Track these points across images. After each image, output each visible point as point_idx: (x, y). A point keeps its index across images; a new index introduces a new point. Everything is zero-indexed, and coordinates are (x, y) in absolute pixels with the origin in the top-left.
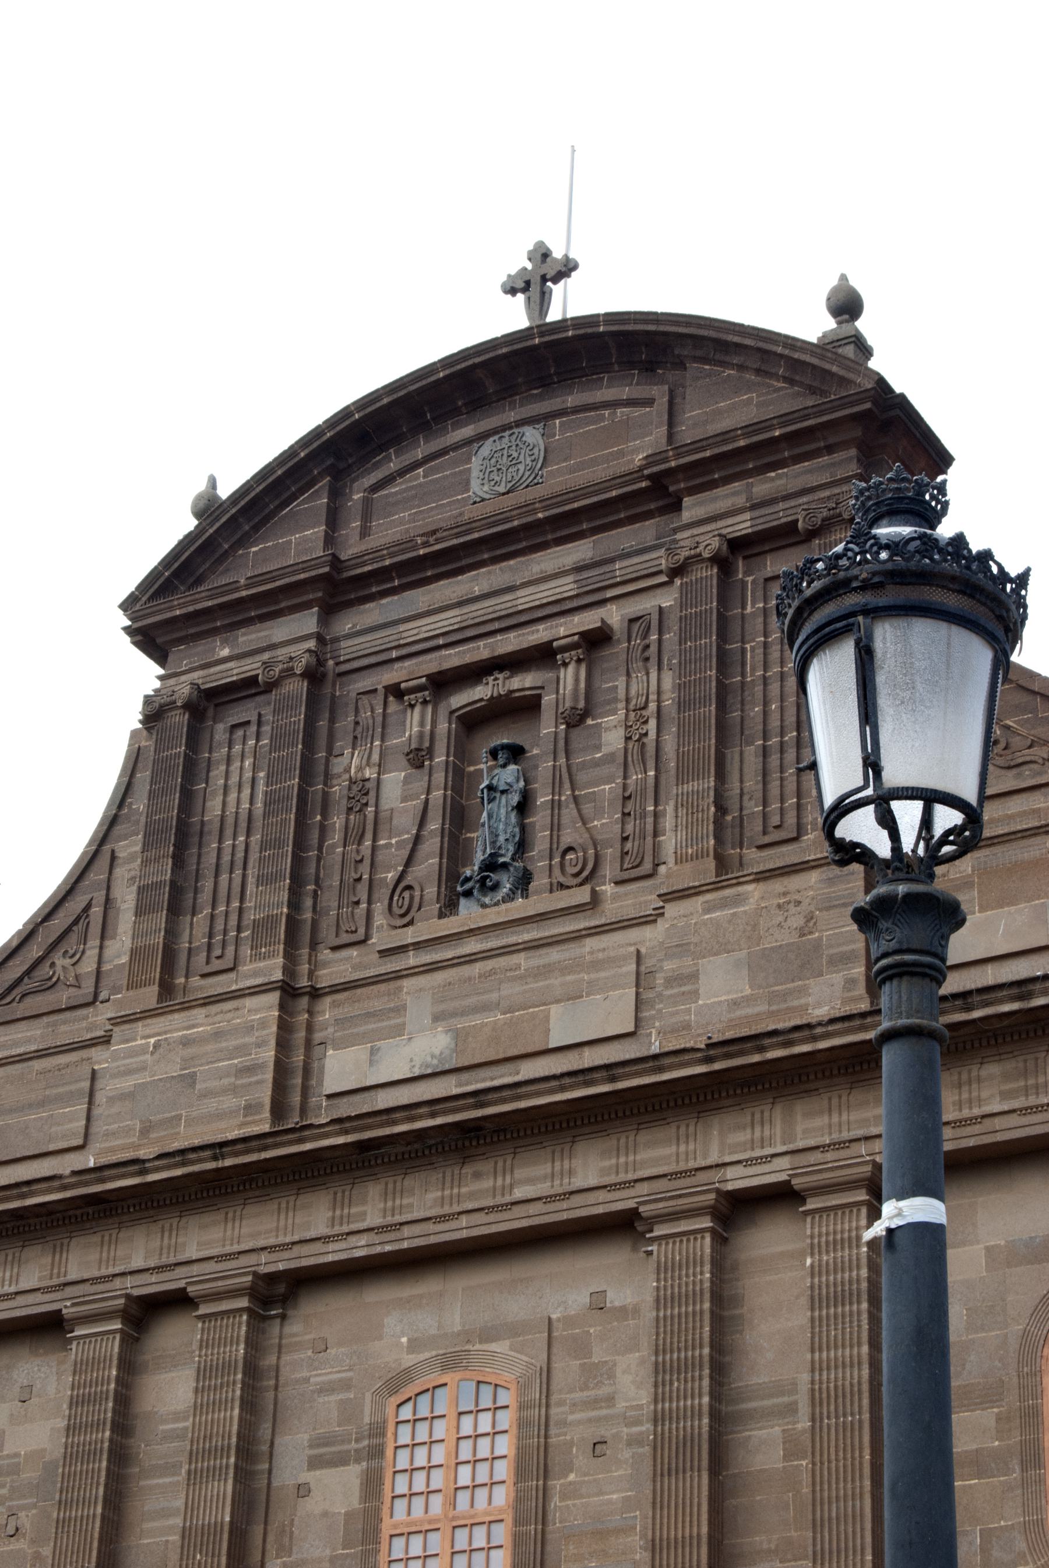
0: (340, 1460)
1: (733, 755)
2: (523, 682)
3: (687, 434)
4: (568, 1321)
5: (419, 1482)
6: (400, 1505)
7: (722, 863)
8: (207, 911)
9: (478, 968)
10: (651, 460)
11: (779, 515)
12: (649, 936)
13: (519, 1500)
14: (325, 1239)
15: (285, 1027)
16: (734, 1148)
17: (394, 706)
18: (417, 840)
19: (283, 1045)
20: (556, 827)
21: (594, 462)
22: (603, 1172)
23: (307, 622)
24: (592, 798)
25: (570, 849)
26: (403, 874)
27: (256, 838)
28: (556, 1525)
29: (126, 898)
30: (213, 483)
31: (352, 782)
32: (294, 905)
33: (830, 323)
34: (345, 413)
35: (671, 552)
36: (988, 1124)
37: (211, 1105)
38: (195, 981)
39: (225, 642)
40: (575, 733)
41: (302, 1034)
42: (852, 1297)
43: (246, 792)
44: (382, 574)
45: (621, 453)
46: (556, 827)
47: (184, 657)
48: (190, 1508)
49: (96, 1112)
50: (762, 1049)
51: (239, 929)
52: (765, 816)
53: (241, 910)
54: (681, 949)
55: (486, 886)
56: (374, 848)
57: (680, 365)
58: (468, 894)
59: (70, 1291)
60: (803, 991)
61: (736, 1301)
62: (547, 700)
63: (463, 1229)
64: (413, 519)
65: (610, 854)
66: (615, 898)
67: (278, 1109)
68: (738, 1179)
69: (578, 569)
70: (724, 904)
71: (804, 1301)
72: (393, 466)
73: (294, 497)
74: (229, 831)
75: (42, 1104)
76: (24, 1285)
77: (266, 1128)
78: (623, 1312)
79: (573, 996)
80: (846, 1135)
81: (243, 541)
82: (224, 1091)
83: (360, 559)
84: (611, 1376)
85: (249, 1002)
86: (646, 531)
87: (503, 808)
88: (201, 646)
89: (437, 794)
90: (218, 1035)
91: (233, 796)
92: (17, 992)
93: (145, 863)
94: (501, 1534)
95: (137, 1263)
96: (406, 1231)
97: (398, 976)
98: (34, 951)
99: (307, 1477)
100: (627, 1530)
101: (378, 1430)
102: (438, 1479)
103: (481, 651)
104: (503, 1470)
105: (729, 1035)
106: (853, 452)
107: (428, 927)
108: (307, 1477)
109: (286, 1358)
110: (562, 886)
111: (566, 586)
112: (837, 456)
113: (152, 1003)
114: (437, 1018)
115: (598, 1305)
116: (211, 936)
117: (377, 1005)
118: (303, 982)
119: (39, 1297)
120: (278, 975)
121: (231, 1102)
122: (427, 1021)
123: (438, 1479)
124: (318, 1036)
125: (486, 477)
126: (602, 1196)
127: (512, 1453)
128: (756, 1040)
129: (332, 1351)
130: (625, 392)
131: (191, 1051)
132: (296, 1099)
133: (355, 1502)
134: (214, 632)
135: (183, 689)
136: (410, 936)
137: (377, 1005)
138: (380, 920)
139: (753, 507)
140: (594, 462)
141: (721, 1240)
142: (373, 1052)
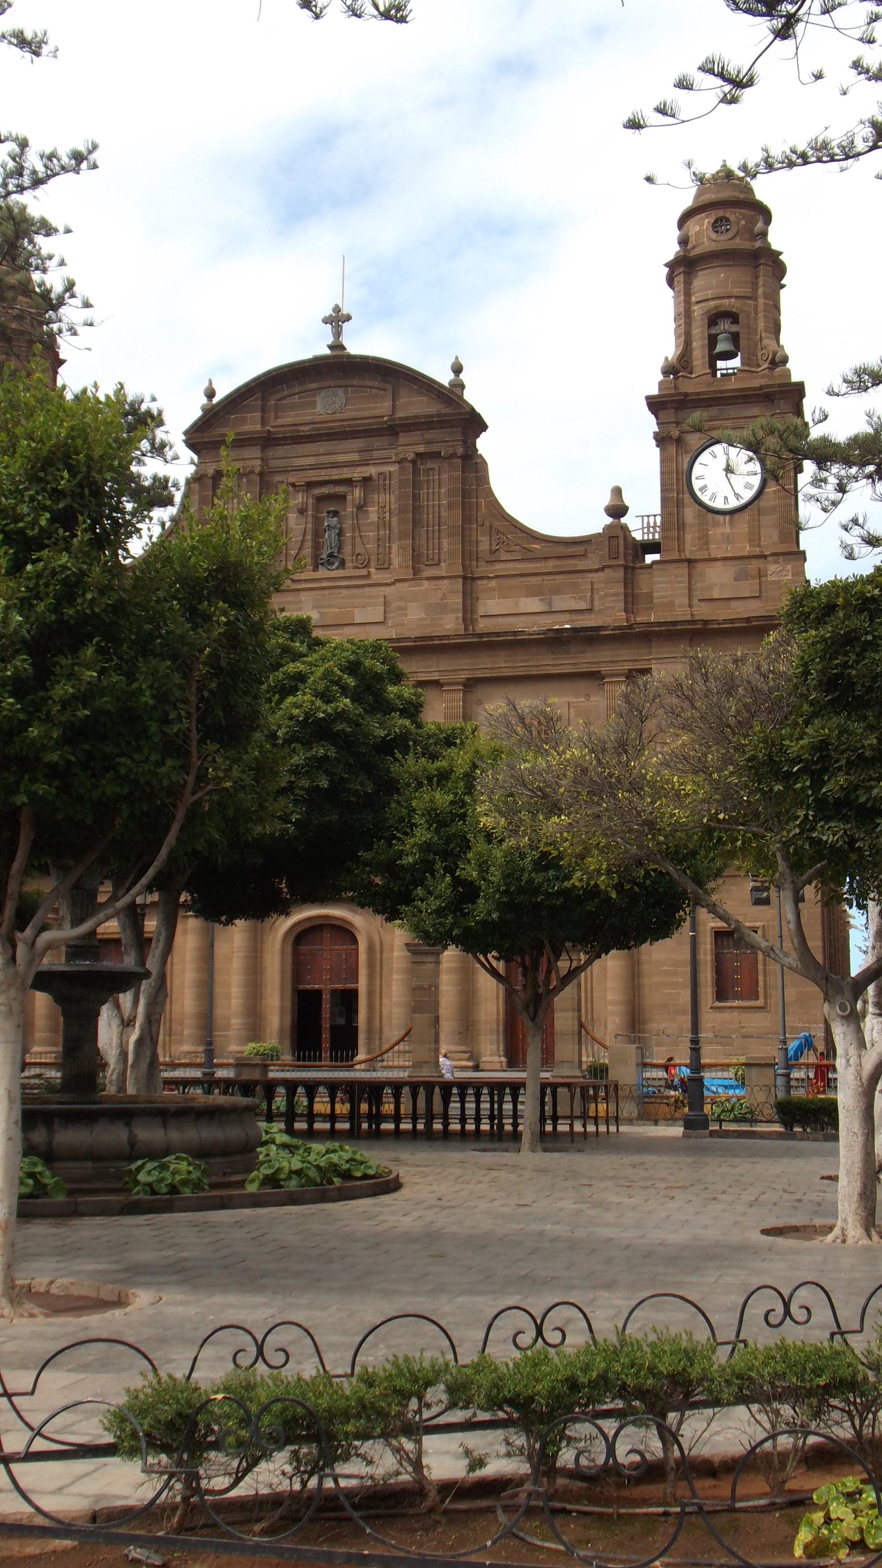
11: (435, 448)
18: (303, 541)
20: (354, 545)
46: (354, 545)
58: (322, 564)
62: (349, 498)
81: (229, 413)
89: (310, 526)
110: (357, 567)
111: (355, 457)
128: (431, 638)
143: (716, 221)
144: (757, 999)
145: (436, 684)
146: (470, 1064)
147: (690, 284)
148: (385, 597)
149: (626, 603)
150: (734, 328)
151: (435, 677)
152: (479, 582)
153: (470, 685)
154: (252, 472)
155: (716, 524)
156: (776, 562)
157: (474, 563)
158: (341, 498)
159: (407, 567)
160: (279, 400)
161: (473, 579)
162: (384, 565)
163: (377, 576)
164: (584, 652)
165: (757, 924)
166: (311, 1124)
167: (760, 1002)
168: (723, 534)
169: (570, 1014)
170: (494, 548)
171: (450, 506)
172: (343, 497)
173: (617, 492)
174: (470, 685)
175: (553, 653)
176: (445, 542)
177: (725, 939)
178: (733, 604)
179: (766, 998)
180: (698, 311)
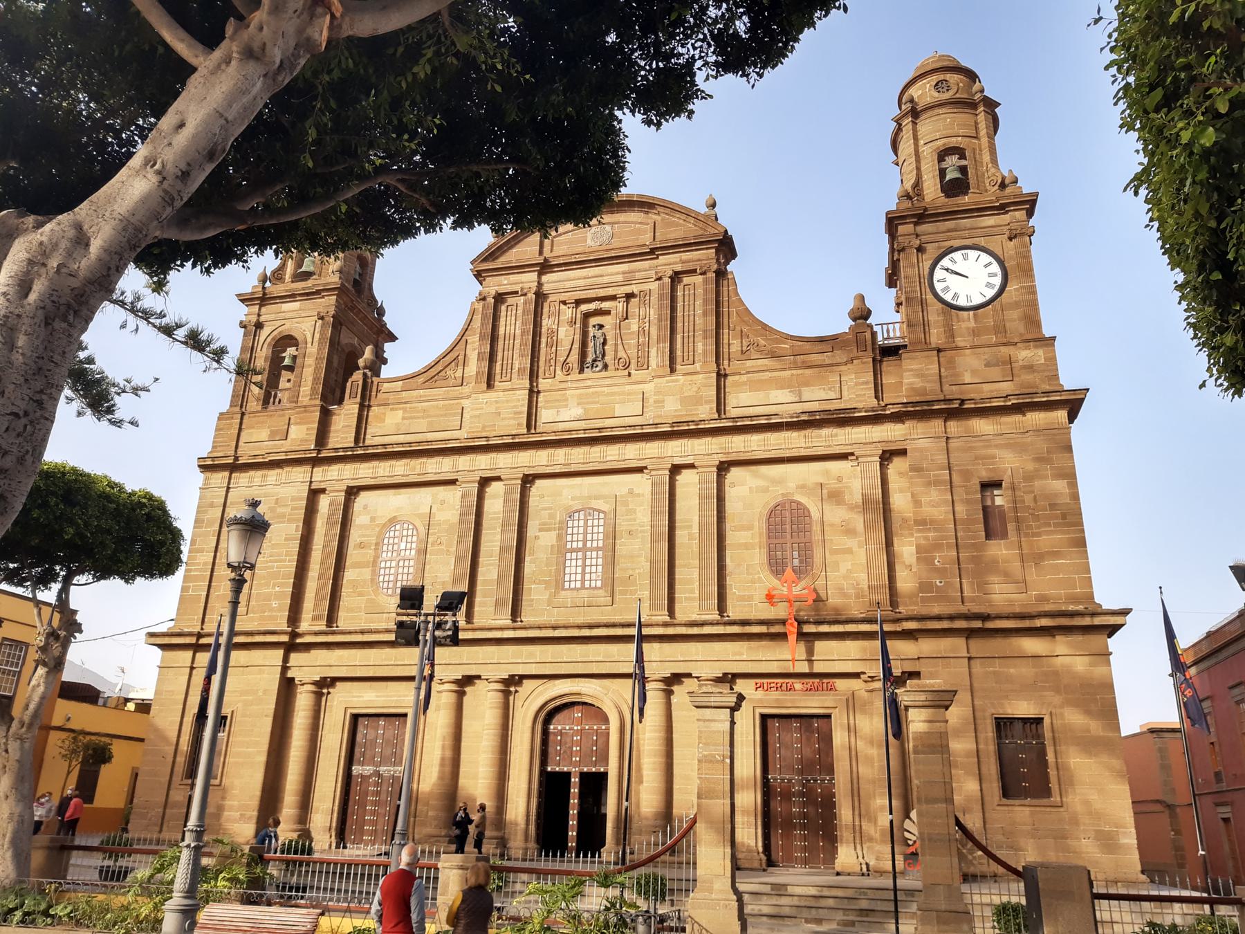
0: (549, 530)
2: (605, 305)
4: (622, 496)
20: (616, 351)
24: (628, 344)
29: (473, 356)
37: (506, 422)
46: (616, 351)
65: (633, 362)
69: (624, 273)
70: (673, 381)
75: (445, 415)
78: (638, 495)
82: (510, 418)
84: (635, 512)
98: (439, 367)
99: (537, 534)
111: (620, 278)
121: (512, 422)
125: (593, 239)
138: (558, 371)
156: (1026, 348)
168: (968, 328)
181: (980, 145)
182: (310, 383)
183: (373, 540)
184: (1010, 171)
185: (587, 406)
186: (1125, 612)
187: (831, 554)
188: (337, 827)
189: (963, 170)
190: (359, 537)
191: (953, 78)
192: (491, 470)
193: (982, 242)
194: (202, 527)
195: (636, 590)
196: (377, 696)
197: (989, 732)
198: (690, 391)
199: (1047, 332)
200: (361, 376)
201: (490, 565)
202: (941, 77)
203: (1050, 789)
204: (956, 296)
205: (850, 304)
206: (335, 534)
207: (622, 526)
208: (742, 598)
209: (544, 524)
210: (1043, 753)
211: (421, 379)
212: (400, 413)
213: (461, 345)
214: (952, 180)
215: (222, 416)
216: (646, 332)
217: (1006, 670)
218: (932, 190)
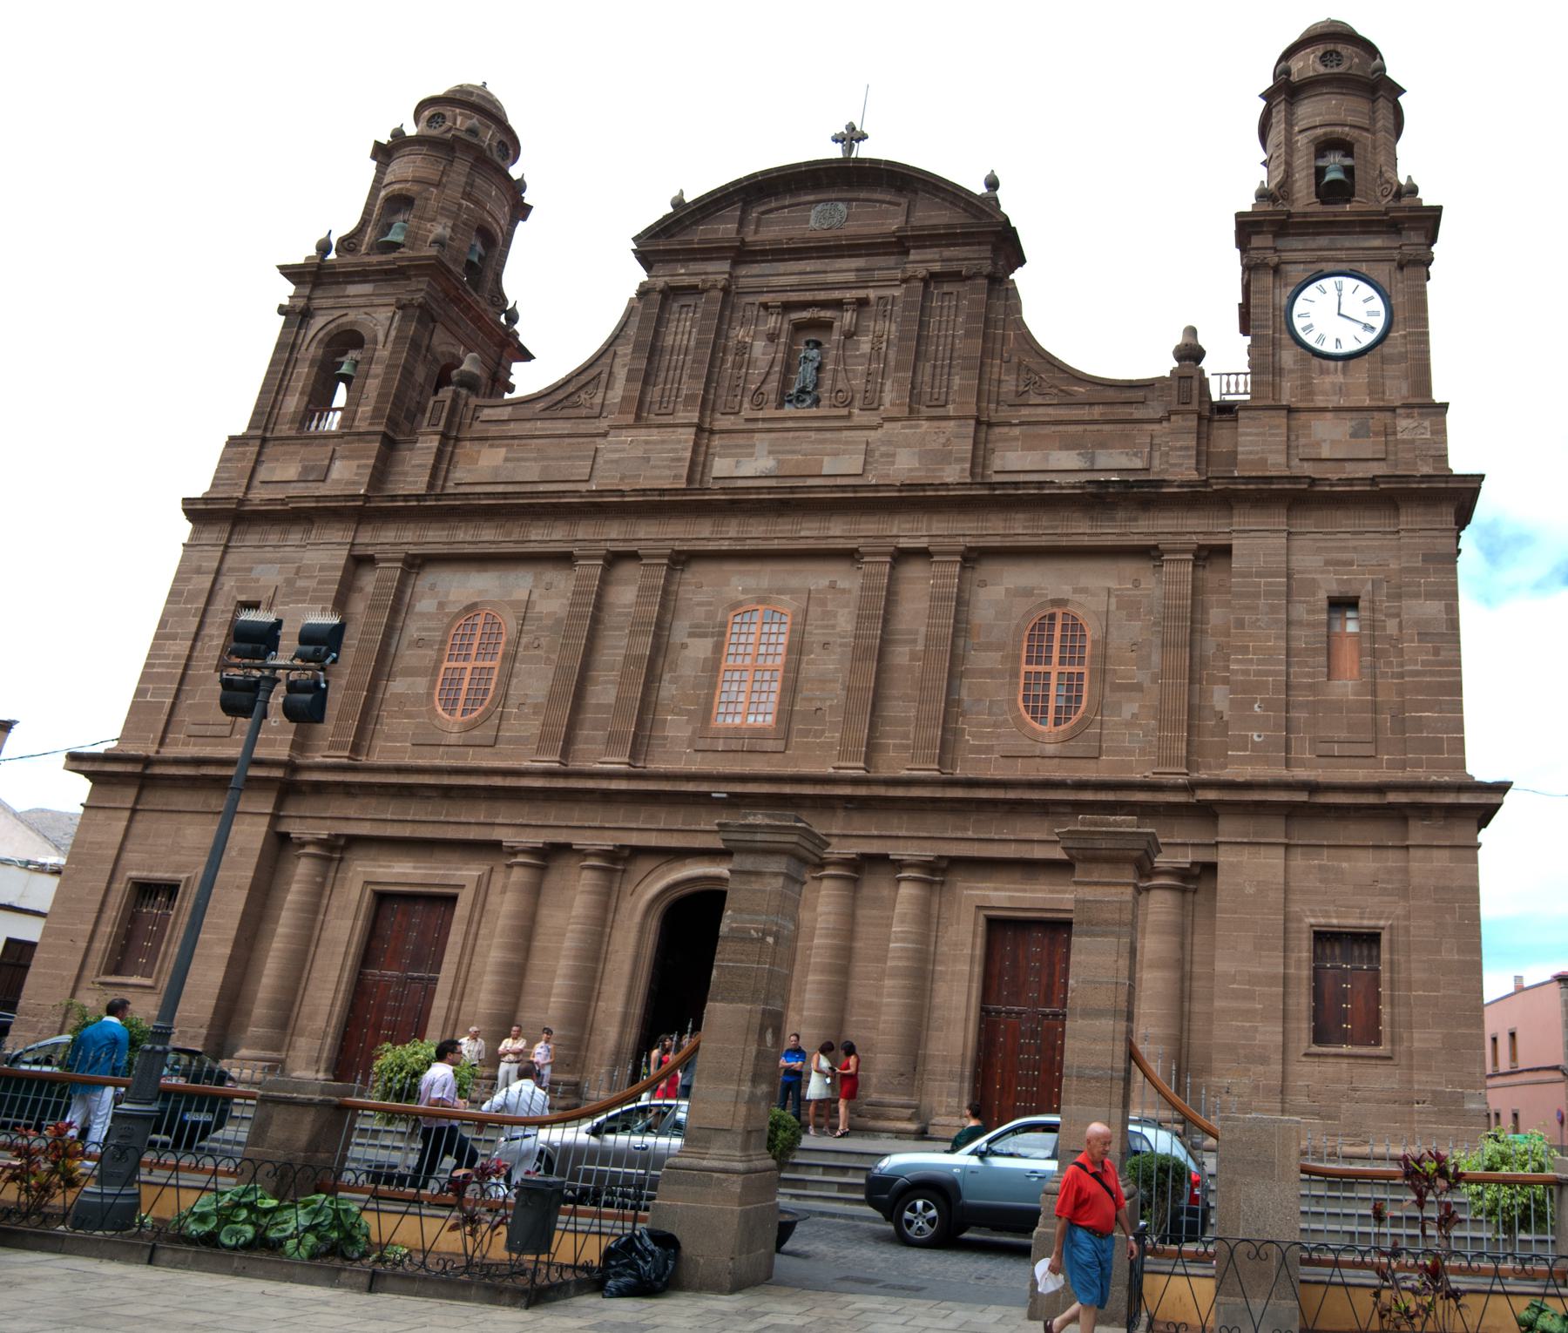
0: (704, 635)
1: (920, 364)
2: (826, 314)
3: (915, 222)
4: (818, 591)
5: (741, 649)
6: (731, 658)
7: (911, 410)
8: (661, 386)
9: (791, 434)
10: (899, 229)
11: (954, 266)
12: (872, 435)
13: (787, 663)
14: (708, 539)
15: (696, 445)
16: (904, 530)
17: (762, 312)
18: (768, 373)
19: (695, 451)
20: (834, 380)
21: (869, 225)
22: (844, 530)
23: (725, 266)
25: (840, 391)
26: (759, 388)
27: (689, 358)
28: (803, 675)
29: (621, 374)
30: (682, 192)
31: (739, 342)
32: (706, 391)
33: (985, 190)
34: (754, 176)
35: (904, 271)
36: (1016, 538)
37: (657, 472)
38: (652, 416)
39: (682, 267)
40: (848, 341)
41: (704, 448)
42: (948, 599)
43: (686, 336)
44: (764, 252)
45: (883, 224)
46: (834, 380)
47: (659, 269)
48: (629, 647)
49: (596, 466)
50: (924, 490)
51: (677, 397)
52: (932, 394)
53: (678, 389)
54: (890, 443)
55: (799, 400)
56: (747, 373)
57: (915, 192)
58: (790, 401)
59: (577, 544)
60: (942, 470)
61: (896, 593)
62: (837, 324)
63: (775, 545)
64: (780, 231)
66: (859, 416)
67: (690, 479)
68: (905, 543)
69: (858, 270)
70: (911, 427)
71: (928, 598)
72: (773, 205)
73: (723, 208)
74: (675, 353)
75: (569, 458)
76: (554, 538)
77: (684, 486)
78: (844, 591)
79: (836, 454)
80: (954, 532)
81: (697, 223)
82: (664, 467)
83: (755, 243)
84: (835, 616)
85: (680, 430)
86: (891, 261)
87: (810, 367)
88: (672, 265)
89: (780, 355)
90: (663, 442)
91: (679, 337)
92: (560, 406)
93: (633, 358)
94: (779, 675)
95: (613, 536)
96: (748, 542)
97: (753, 431)
98: (571, 389)
99: (688, 641)
100: (834, 681)
101: (724, 625)
102: (750, 649)
103: (808, 296)
104: (781, 649)
105: (908, 482)
106: (989, 247)
107: (769, 412)
108: (688, 641)
109: (681, 588)
111: (851, 277)
112: (982, 248)
113: (631, 422)
114: (770, 453)
115: (833, 586)
116: (662, 397)
117: (742, 442)
118: (707, 426)
119: (561, 544)
120: (696, 420)
121: (667, 472)
122: (765, 453)
123: (750, 649)
124: (711, 451)
126: (842, 541)
127: (786, 643)
128: (923, 486)
129: (705, 588)
130: (888, 198)
131: (647, 447)
132: (698, 477)
133: (709, 654)
134: (678, 261)
135: (660, 283)
136: (760, 414)
137: (742, 442)
138: (746, 405)
139: (943, 261)
140: (869, 225)
141: (893, 568)
142: (738, 462)
143: (1324, 55)
144: (1378, 1043)
145: (923, 554)
146: (912, 1126)
147: (1293, 114)
148: (867, 443)
149: (1198, 462)
150: (1348, 162)
151: (922, 543)
152: (997, 430)
153: (973, 557)
154: (714, 287)
155: (1323, 371)
156: (1408, 416)
157: (993, 406)
158: (827, 326)
159: (901, 405)
160: (764, 213)
161: (990, 425)
162: (871, 405)
163: (859, 417)
164: (1136, 519)
165: (1382, 923)
166: (636, 1214)
167: (1382, 1050)
168: (1333, 384)
169: (1106, 1024)
170: (1021, 389)
171: (968, 335)
172: (827, 326)
173: (1191, 332)
174: (973, 557)
175: (1092, 518)
176: (957, 380)
177: (1328, 946)
178: (1347, 465)
179: (1393, 1042)
180: (1302, 140)
181: (1374, 141)
182: (372, 402)
183: (438, 635)
184: (1409, 177)
185: (781, 457)
186: (1503, 788)
187: (1112, 690)
188: (329, 1059)
189: (1349, 171)
190: (418, 629)
191: (1345, 50)
192: (624, 540)
193: (1364, 268)
194: (179, 602)
195: (823, 731)
196: (414, 868)
197: (1303, 950)
198: (936, 444)
199: (1438, 397)
200: (450, 394)
201: (606, 682)
202: (1331, 47)
203: (1379, 1032)
204: (1321, 338)
205: (1178, 339)
206: (380, 624)
207: (815, 634)
208: (978, 750)
209: (697, 626)
210: (1376, 981)
211: (540, 405)
212: (502, 452)
213: (606, 360)
214: (1332, 182)
215: (233, 441)
216: (882, 355)
217: (1335, 863)
218: (1304, 197)
